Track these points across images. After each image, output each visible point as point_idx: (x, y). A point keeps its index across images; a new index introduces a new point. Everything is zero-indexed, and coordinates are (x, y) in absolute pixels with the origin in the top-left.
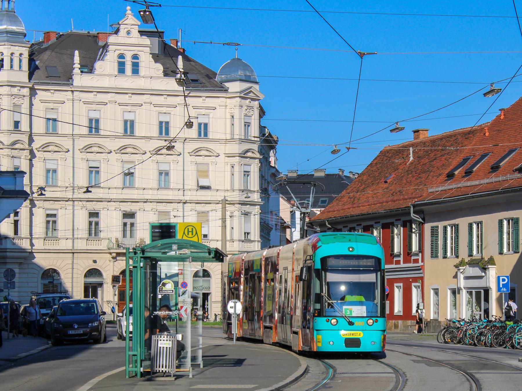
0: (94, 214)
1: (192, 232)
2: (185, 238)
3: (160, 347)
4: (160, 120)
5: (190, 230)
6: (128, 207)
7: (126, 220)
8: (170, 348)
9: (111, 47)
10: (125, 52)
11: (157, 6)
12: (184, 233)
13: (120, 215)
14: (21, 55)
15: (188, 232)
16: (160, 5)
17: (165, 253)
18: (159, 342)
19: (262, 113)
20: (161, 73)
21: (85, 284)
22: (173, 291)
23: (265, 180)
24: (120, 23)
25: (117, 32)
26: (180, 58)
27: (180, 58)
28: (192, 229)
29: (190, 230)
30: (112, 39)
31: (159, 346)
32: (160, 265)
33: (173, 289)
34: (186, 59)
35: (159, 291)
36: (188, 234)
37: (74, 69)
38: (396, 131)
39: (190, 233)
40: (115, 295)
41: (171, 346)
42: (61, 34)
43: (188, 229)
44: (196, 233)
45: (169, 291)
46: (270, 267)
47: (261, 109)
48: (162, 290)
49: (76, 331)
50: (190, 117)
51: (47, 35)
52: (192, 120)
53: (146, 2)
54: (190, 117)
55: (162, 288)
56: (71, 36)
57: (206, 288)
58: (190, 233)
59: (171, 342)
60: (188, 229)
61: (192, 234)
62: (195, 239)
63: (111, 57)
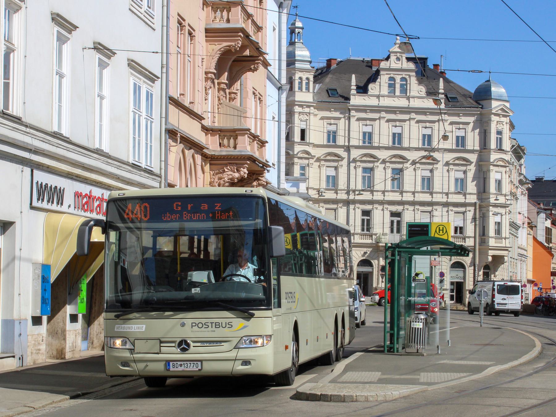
0: (366, 213)
1: (443, 230)
2: (436, 236)
3: (413, 328)
4: (327, 175)
5: (441, 229)
6: (368, 207)
7: (393, 218)
8: (421, 328)
9: (382, 73)
10: (395, 76)
11: (416, 38)
12: (436, 231)
13: (387, 214)
14: (308, 79)
15: (439, 230)
16: (419, 38)
17: (419, 248)
18: (412, 323)
19: (512, 126)
20: (423, 94)
21: (357, 272)
22: (424, 280)
23: (514, 185)
24: (390, 51)
25: (388, 58)
26: (441, 80)
27: (441, 80)
28: (443, 228)
29: (441, 229)
30: (383, 65)
31: (412, 326)
32: (415, 258)
33: (424, 279)
34: (446, 81)
35: (413, 280)
36: (439, 232)
37: (351, 90)
38: (94, 305)
39: (441, 232)
40: (383, 282)
41: (422, 327)
42: (339, 60)
43: (439, 228)
44: (446, 231)
45: (421, 281)
46: (255, 308)
47: (511, 123)
48: (415, 279)
49: (60, 353)
50: (445, 131)
51: (329, 62)
52: (447, 134)
53: (407, 35)
54: (445, 131)
55: (415, 278)
56: (349, 62)
57: (461, 278)
58: (441, 232)
59: (422, 324)
60: (439, 228)
61: (443, 232)
62: (445, 237)
63: (384, 78)
